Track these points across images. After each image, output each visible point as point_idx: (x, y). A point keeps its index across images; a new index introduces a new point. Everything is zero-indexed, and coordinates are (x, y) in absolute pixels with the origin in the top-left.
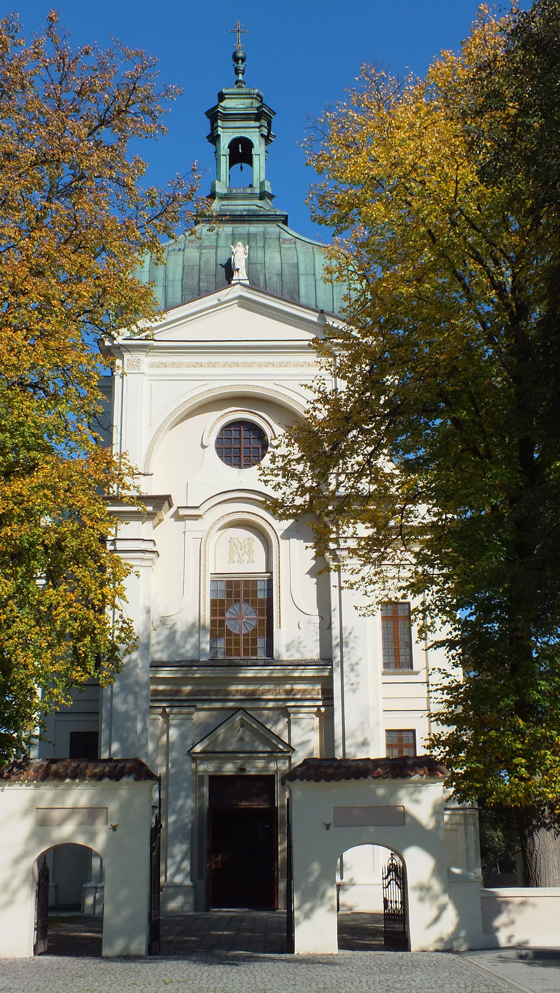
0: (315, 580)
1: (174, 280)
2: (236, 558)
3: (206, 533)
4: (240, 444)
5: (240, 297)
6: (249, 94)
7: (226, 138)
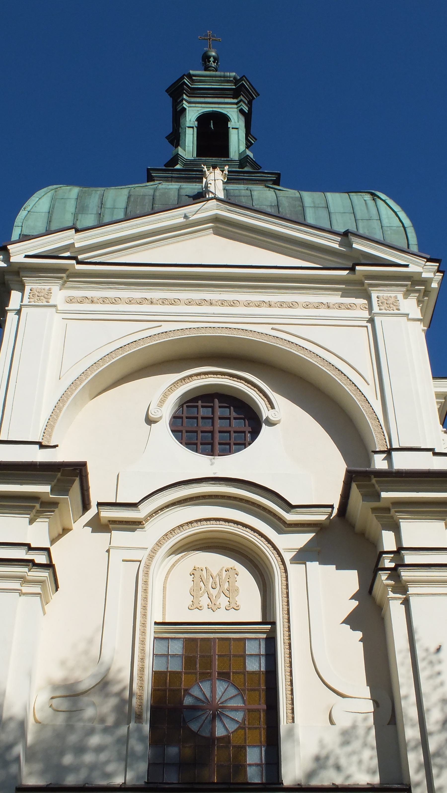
0: (359, 634)
1: (114, 208)
2: (204, 601)
3: (148, 552)
4: (213, 425)
5: (216, 219)
6: (224, 77)
7: (192, 114)
